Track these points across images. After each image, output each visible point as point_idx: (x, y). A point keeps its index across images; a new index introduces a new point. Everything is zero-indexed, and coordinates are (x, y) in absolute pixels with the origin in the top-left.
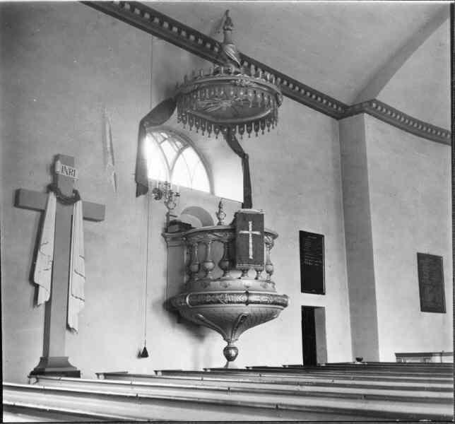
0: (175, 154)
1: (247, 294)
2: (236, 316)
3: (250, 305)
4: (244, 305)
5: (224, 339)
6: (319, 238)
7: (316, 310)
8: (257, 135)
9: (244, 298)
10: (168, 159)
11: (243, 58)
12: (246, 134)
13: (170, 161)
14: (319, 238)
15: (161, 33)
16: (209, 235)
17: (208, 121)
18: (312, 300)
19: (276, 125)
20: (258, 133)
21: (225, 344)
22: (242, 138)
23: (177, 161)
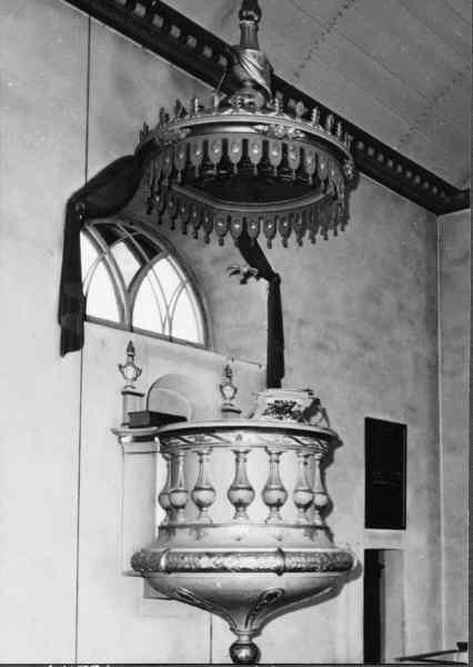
0: (293, 523)
1: (281, 553)
2: (258, 594)
3: (285, 575)
4: (275, 575)
5: (232, 629)
6: (400, 430)
7: (386, 553)
8: (326, 239)
9: (277, 562)
10: (124, 277)
11: (277, 85)
12: (278, 238)
13: (127, 283)
14: (400, 430)
15: (111, 15)
16: (207, 437)
17: (335, 115)
18: (382, 538)
19: (343, 230)
20: (273, 241)
21: (233, 638)
22: (270, 246)
23: (234, 475)
